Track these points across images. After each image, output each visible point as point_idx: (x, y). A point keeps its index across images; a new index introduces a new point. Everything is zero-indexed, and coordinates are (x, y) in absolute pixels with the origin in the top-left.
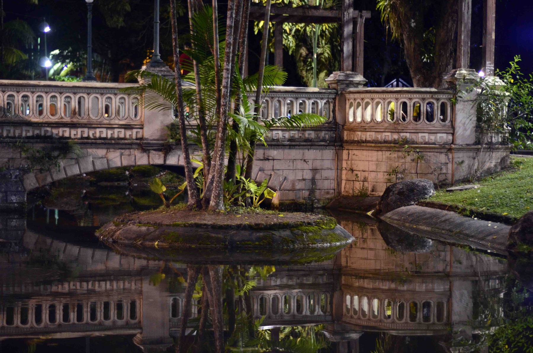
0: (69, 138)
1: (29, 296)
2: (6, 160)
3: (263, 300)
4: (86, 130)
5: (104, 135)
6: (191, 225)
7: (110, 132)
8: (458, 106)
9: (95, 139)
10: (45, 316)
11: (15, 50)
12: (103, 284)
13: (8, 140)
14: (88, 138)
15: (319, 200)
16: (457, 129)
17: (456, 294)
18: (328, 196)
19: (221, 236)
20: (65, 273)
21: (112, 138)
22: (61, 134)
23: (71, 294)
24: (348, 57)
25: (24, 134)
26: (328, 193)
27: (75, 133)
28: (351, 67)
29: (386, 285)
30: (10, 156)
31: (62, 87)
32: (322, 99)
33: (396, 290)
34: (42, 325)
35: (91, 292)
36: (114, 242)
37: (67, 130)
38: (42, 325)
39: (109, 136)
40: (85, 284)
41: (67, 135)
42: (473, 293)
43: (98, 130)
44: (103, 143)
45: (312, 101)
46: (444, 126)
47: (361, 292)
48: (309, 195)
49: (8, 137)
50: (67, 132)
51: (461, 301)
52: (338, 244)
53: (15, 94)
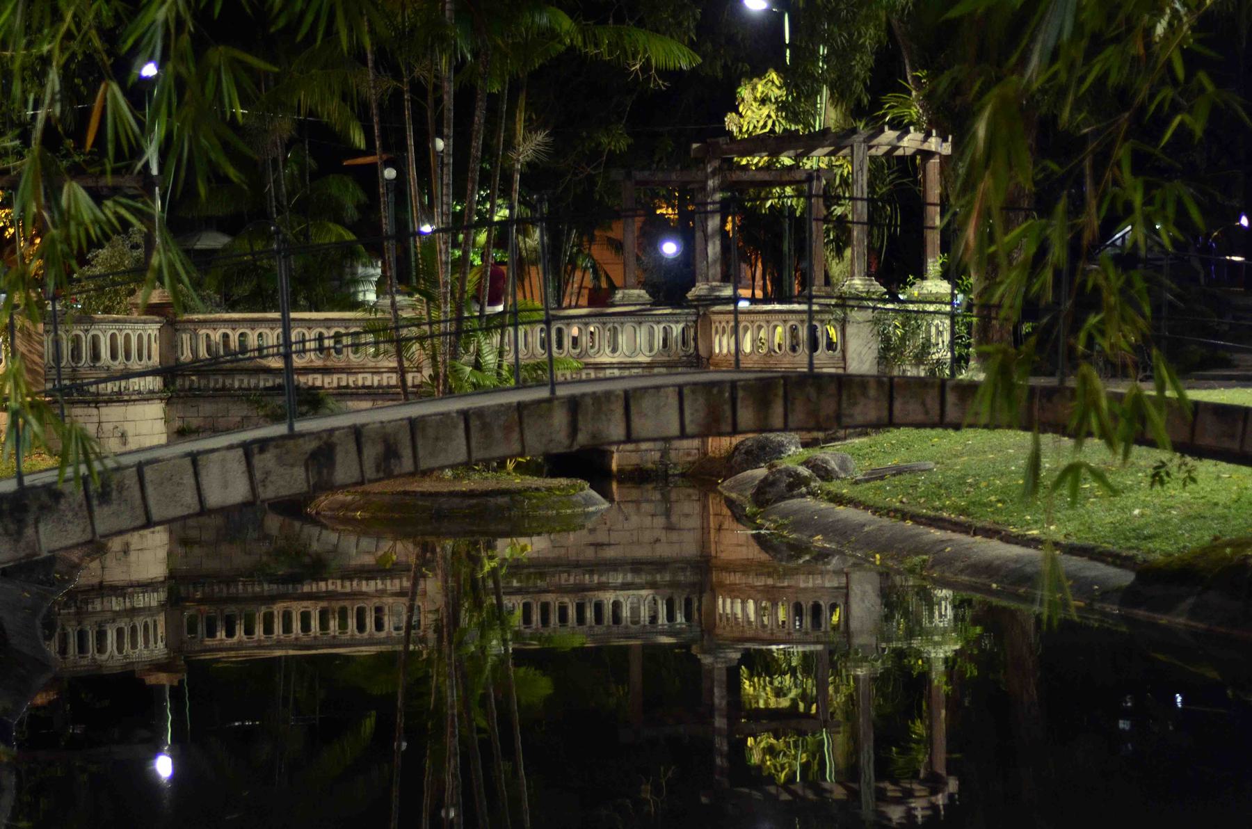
0: (322, 388)
1: (273, 599)
2: (239, 419)
3: (599, 607)
4: (344, 376)
5: (368, 383)
6: (398, 493)
7: (376, 378)
8: (850, 330)
9: (357, 388)
10: (296, 626)
11: (331, 225)
12: (372, 583)
13: (240, 392)
14: (347, 387)
15: (675, 465)
16: (849, 361)
17: (856, 590)
18: (690, 459)
19: (428, 504)
20: (317, 568)
21: (380, 387)
22: (310, 383)
23: (331, 596)
24: (715, 262)
25: (262, 384)
26: (689, 454)
27: (331, 381)
28: (719, 276)
29: (760, 582)
30: (245, 413)
31: (310, 320)
32: (677, 322)
33: (774, 587)
34: (293, 636)
35: (354, 595)
36: (318, 513)
37: (319, 377)
38: (293, 636)
39: (376, 383)
40: (347, 584)
41: (318, 383)
42: (882, 589)
43: (360, 376)
44: (366, 394)
45: (661, 326)
46: (832, 357)
47: (733, 592)
48: (662, 457)
49: (240, 388)
50: (318, 380)
51: (863, 601)
52: (569, 511)
53: (248, 331)
